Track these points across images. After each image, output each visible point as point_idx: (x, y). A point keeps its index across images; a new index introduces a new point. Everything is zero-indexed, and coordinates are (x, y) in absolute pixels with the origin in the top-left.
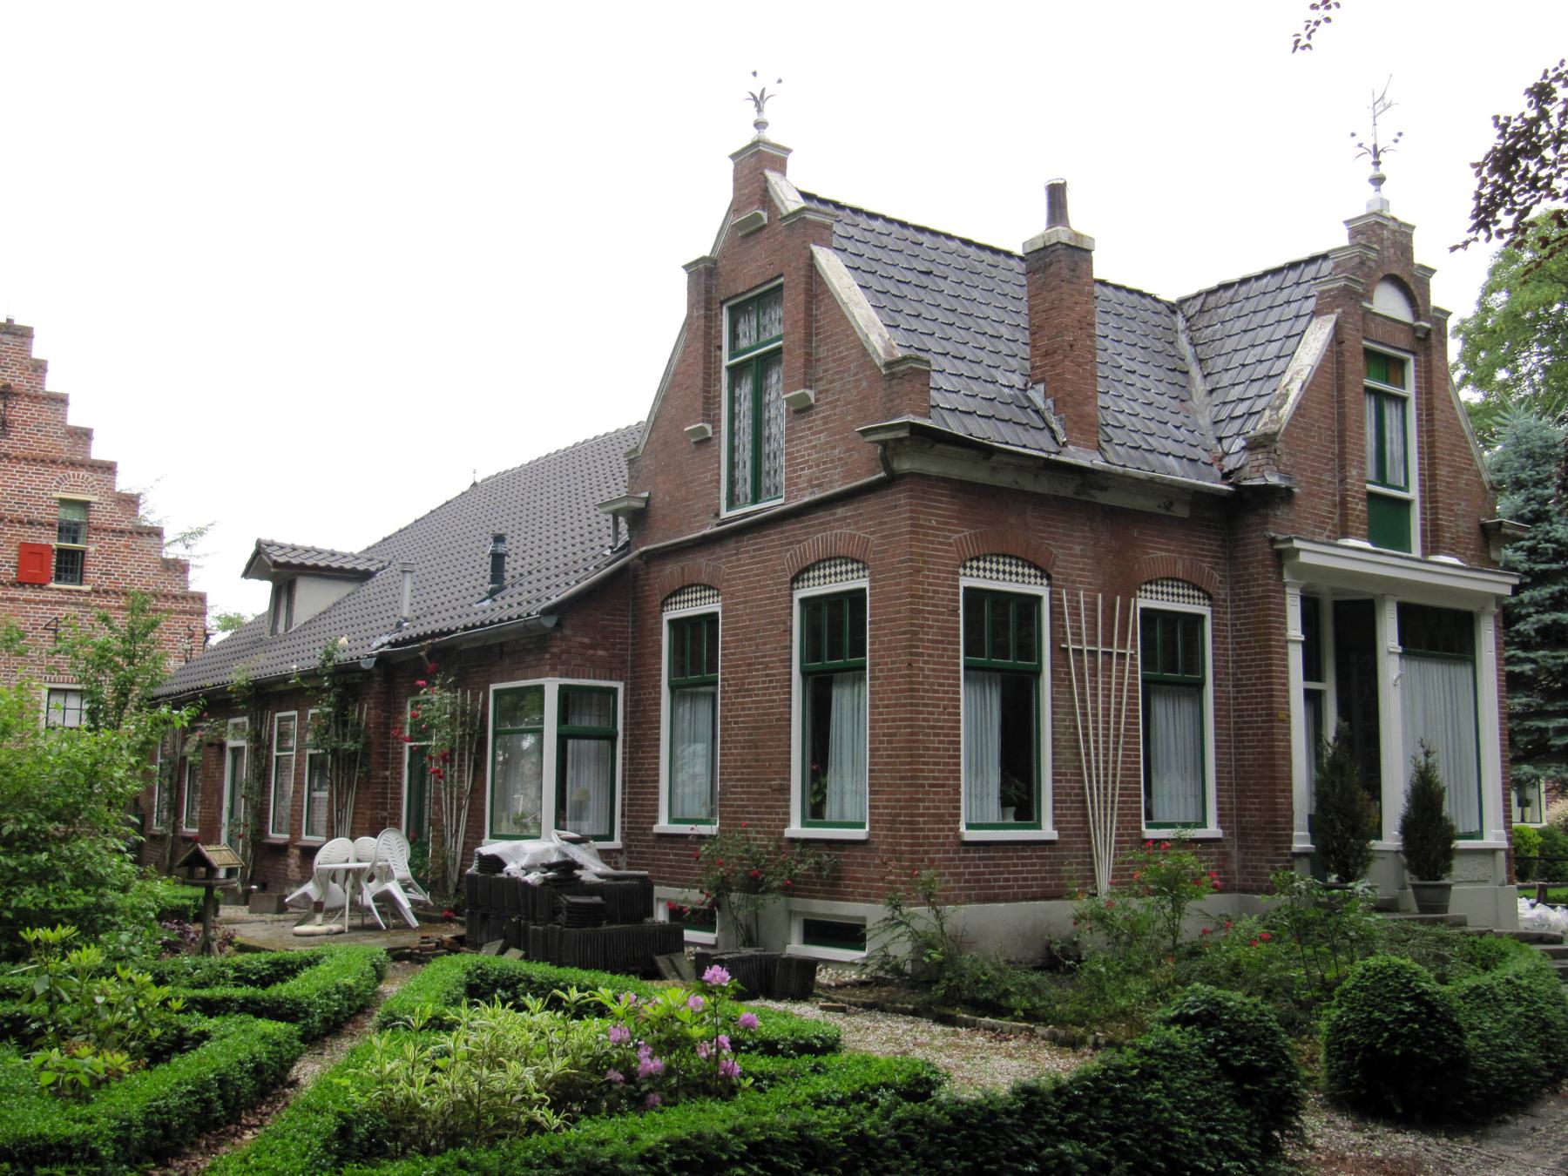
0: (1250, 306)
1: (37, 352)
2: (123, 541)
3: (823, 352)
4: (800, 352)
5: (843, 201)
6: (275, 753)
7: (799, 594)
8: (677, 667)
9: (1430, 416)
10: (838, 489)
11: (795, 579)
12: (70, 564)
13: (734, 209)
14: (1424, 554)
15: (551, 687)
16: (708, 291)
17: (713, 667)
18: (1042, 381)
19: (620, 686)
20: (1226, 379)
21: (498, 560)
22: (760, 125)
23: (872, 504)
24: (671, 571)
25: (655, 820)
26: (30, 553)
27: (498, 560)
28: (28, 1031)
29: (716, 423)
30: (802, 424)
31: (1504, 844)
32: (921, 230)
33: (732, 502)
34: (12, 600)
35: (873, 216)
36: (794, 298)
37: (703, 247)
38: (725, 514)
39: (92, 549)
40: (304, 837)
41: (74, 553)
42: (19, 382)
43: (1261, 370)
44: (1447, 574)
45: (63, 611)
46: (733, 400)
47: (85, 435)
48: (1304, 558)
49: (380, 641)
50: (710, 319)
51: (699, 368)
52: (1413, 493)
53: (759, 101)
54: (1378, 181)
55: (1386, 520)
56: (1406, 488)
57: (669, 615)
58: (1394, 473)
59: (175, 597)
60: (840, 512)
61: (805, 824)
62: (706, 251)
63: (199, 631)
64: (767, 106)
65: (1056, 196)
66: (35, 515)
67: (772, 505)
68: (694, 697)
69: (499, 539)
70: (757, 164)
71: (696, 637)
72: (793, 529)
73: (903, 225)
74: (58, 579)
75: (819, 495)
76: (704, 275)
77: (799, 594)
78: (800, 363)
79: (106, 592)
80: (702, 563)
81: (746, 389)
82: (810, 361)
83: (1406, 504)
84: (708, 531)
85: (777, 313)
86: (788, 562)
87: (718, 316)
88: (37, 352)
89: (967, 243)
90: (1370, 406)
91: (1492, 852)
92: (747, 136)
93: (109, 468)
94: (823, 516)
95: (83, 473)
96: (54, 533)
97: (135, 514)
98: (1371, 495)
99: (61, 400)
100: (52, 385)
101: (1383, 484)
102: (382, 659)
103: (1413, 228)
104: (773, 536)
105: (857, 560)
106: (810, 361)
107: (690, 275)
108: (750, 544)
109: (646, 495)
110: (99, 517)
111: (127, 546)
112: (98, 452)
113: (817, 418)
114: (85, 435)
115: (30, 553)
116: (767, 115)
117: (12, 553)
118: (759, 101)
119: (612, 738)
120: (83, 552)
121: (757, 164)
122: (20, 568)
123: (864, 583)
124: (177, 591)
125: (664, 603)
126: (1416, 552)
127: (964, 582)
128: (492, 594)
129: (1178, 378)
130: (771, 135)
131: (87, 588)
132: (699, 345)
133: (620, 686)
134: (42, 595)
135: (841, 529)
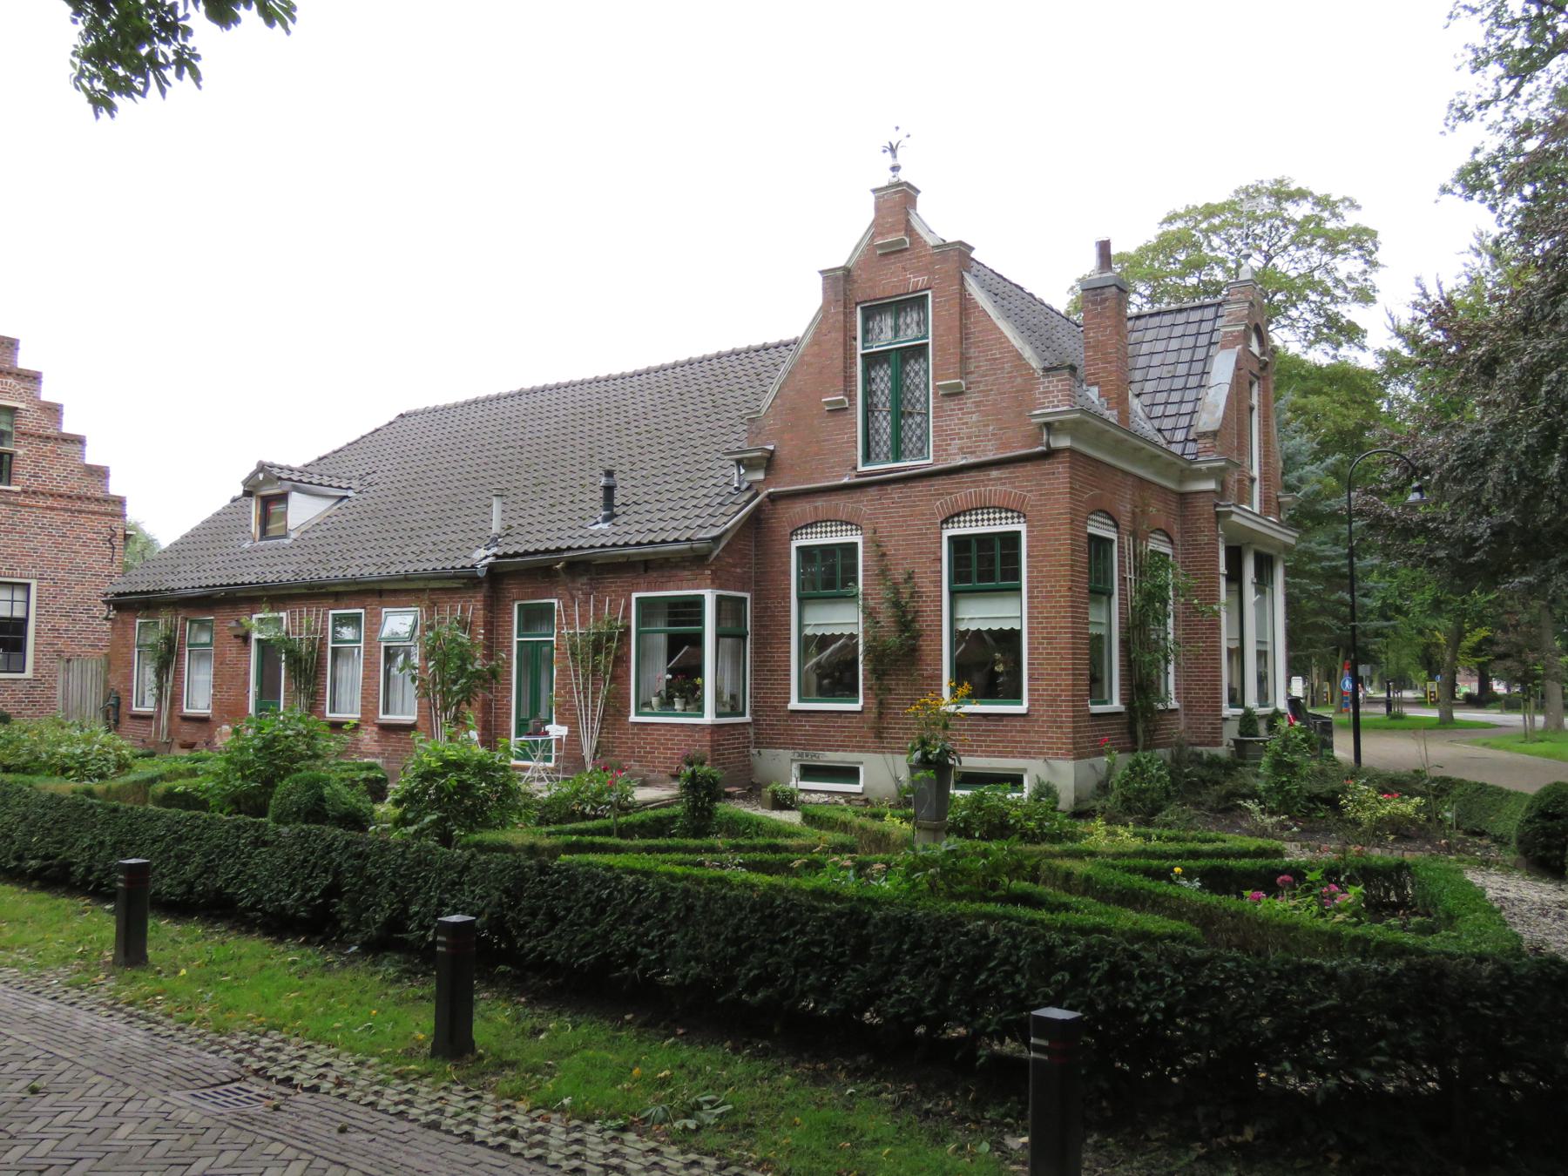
2: (50, 446)
3: (973, 352)
6: (330, 645)
7: (947, 533)
10: (990, 457)
11: (946, 521)
13: (877, 228)
15: (709, 597)
18: (1096, 384)
21: (609, 490)
24: (803, 509)
27: (609, 490)
29: (851, 396)
30: (950, 404)
33: (867, 458)
37: (840, 257)
38: (861, 468)
39: (20, 452)
40: (381, 716)
46: (868, 381)
48: (1234, 518)
50: (848, 315)
59: (97, 500)
60: (994, 474)
62: (841, 262)
63: (120, 532)
64: (899, 152)
67: (928, 462)
68: (1098, 602)
69: (609, 474)
70: (898, 201)
75: (972, 460)
77: (947, 533)
79: (34, 493)
80: (843, 504)
81: (883, 375)
84: (846, 480)
86: (940, 506)
87: (853, 313)
92: (884, 179)
93: (34, 378)
94: (981, 476)
95: (10, 380)
97: (59, 422)
103: (918, 192)
104: (920, 488)
107: (824, 279)
109: (771, 447)
110: (28, 423)
111: (52, 452)
113: (969, 402)
118: (893, 150)
120: (11, 455)
121: (898, 201)
124: (99, 495)
125: (794, 533)
130: (903, 176)
131: (18, 489)
133: (747, 595)
135: (996, 485)
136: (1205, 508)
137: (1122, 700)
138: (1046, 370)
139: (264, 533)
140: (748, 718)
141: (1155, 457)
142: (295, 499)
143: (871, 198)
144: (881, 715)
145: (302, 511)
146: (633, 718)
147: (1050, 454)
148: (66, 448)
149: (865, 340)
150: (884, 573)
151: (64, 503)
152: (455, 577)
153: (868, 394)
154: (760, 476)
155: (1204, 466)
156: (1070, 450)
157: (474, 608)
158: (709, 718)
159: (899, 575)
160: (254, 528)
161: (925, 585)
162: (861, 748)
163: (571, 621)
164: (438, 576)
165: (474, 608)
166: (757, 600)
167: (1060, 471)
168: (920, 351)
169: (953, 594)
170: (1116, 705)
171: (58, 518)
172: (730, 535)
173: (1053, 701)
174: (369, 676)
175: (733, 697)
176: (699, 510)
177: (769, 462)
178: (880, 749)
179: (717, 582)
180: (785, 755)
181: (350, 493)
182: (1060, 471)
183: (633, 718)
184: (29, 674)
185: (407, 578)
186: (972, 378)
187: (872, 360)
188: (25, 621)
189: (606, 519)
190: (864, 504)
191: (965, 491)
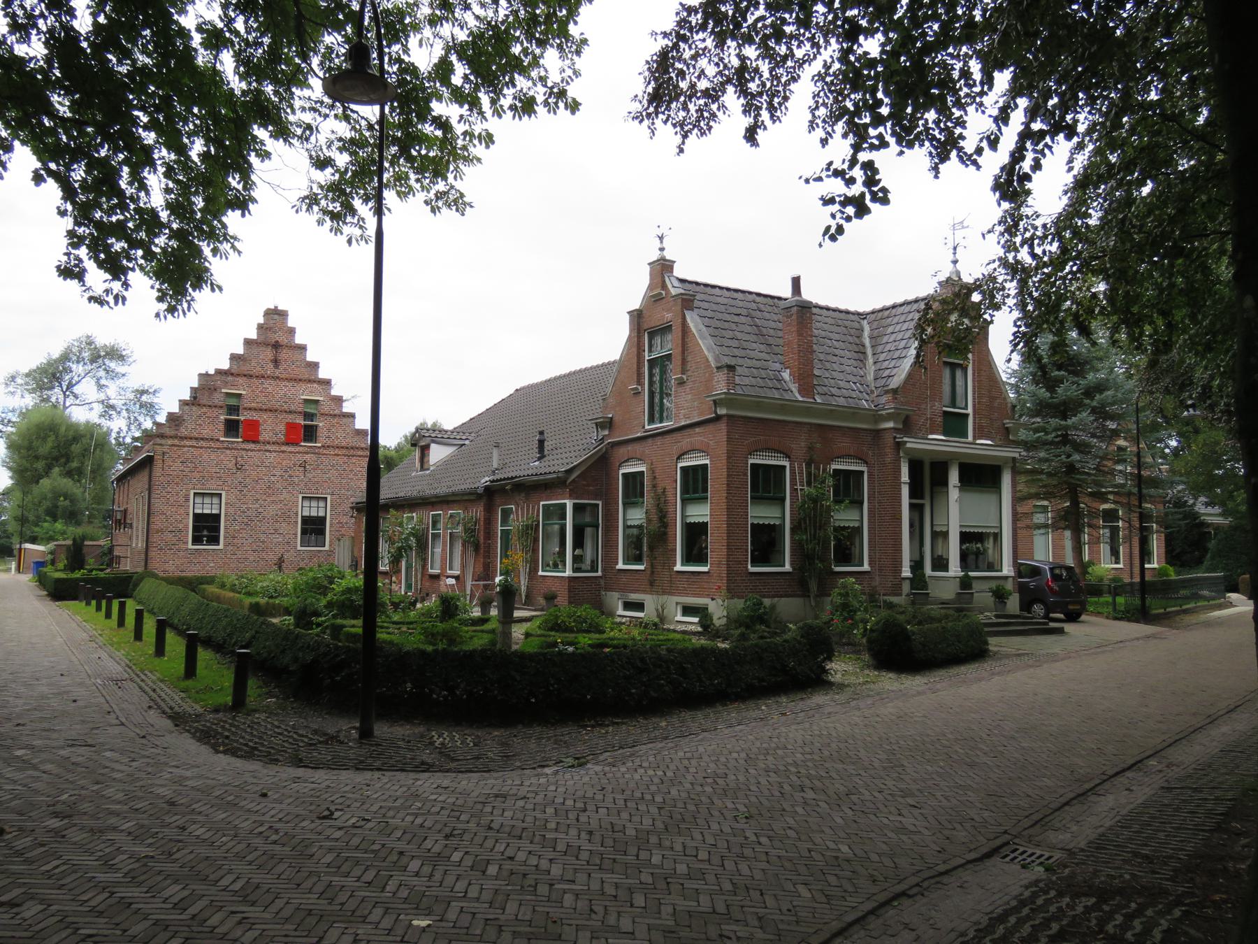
0: (896, 320)
1: (291, 323)
3: (689, 358)
4: (679, 358)
5: (699, 280)
8: (626, 495)
9: (980, 370)
11: (678, 458)
12: (310, 433)
13: (650, 288)
14: (975, 438)
15: (569, 504)
16: (639, 324)
17: (642, 496)
19: (600, 503)
20: (882, 357)
21: (541, 442)
22: (662, 249)
23: (711, 427)
24: (622, 452)
25: (617, 563)
26: (291, 427)
27: (541, 442)
28: (1215, 390)
30: (680, 389)
31: (1012, 574)
32: (736, 291)
33: (651, 420)
34: (283, 452)
35: (714, 287)
36: (677, 329)
37: (636, 305)
41: (312, 426)
42: (283, 339)
43: (897, 354)
44: (981, 446)
45: (307, 457)
46: (651, 375)
47: (315, 366)
48: (908, 445)
49: (485, 480)
51: (635, 360)
52: (970, 410)
53: (661, 238)
54: (955, 262)
55: (954, 424)
56: (966, 408)
57: (622, 471)
58: (960, 401)
60: (697, 430)
61: (683, 565)
62: (637, 307)
65: (796, 282)
66: (293, 408)
67: (668, 424)
69: (541, 433)
70: (662, 267)
71: (634, 482)
72: (677, 435)
73: (728, 289)
74: (305, 441)
76: (637, 317)
77: (680, 465)
78: (679, 363)
80: (637, 448)
81: (657, 371)
82: (684, 362)
83: (967, 415)
85: (669, 337)
86: (675, 451)
88: (291, 323)
89: (759, 295)
90: (947, 373)
91: (1006, 578)
92: (655, 256)
93: (327, 383)
94: (690, 431)
96: (302, 417)
98: (945, 412)
99: (303, 348)
100: (299, 340)
101: (954, 407)
102: (487, 489)
104: (668, 438)
105: (703, 451)
106: (684, 362)
108: (659, 441)
112: (322, 374)
114: (315, 366)
115: (291, 427)
116: (665, 245)
117: (282, 427)
118: (661, 238)
119: (597, 527)
121: (662, 267)
122: (287, 434)
123: (707, 462)
126: (970, 439)
127: (751, 461)
128: (539, 459)
129: (861, 356)
132: (635, 350)
133: (600, 503)
134: (298, 449)
135: (698, 437)
136: (888, 440)
137: (792, 565)
138: (718, 368)
139: (422, 468)
140: (600, 573)
141: (854, 413)
142: (433, 446)
143: (648, 268)
144: (653, 573)
145: (438, 454)
146: (540, 573)
147: (718, 418)
148: (345, 420)
149: (650, 351)
150: (654, 486)
151: (344, 451)
152: (470, 494)
153: (651, 383)
154: (606, 432)
155: (884, 412)
156: (728, 416)
157: (478, 512)
158: (568, 572)
159: (660, 491)
160: (418, 464)
161: (670, 498)
162: (644, 592)
163: (518, 515)
164: (464, 494)
165: (478, 512)
166: (606, 505)
167: (723, 426)
168: (669, 357)
169: (683, 500)
170: (788, 567)
171: (340, 460)
172: (583, 468)
173: (720, 563)
174: (444, 550)
175: (592, 562)
176: (569, 454)
177: (608, 424)
178: (651, 593)
179: (571, 497)
180: (616, 595)
181: (467, 442)
182: (723, 426)
183: (540, 573)
184: (327, 548)
185: (453, 494)
186: (689, 373)
187: (652, 363)
188: (325, 518)
189: (539, 459)
190: (646, 448)
191: (685, 441)
